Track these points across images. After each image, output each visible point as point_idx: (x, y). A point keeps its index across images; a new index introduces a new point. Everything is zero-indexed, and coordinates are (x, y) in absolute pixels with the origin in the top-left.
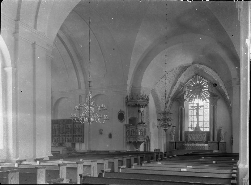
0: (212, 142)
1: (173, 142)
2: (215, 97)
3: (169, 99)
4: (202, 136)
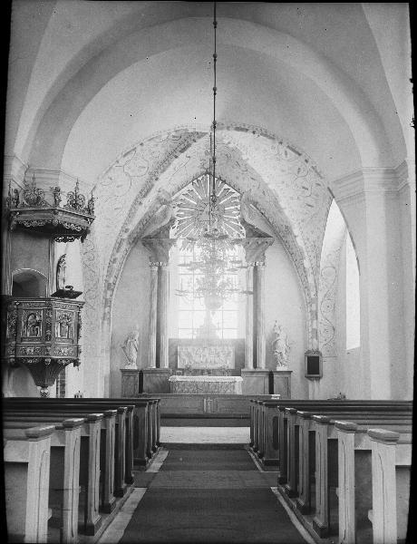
0: (252, 372)
1: (135, 371)
2: (263, 240)
3: (125, 236)
4: (221, 354)
